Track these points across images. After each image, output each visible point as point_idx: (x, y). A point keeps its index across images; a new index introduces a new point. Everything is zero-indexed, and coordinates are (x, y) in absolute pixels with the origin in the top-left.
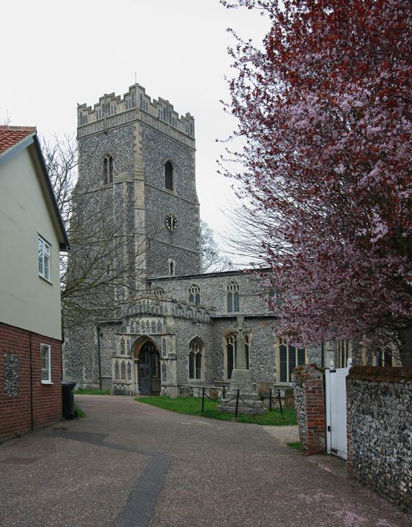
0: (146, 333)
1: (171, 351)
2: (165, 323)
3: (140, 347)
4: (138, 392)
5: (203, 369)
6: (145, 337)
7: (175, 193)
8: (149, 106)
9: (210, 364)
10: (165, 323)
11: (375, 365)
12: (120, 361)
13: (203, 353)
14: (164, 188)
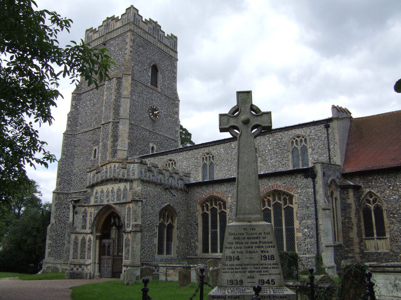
0: (111, 202)
1: (135, 221)
2: (131, 188)
4: (97, 274)
6: (108, 207)
7: (159, 90)
8: (141, 22)
9: (183, 236)
12: (80, 237)
13: (175, 225)
14: (149, 84)
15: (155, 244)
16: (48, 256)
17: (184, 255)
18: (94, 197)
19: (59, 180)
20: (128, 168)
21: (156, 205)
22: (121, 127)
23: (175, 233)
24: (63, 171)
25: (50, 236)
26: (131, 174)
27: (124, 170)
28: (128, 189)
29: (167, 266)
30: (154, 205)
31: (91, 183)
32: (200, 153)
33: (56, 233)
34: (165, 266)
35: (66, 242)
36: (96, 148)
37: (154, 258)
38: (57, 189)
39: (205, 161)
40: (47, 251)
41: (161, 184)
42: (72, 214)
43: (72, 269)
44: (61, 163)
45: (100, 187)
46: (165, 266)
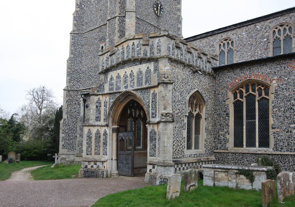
0: (130, 89)
2: (156, 69)
3: (120, 110)
5: (203, 135)
6: (127, 94)
10: (156, 69)
11: (48, 155)
12: (94, 130)
13: (203, 115)
15: (184, 138)
16: (62, 148)
17: (211, 149)
18: (108, 83)
19: (69, 78)
20: (151, 43)
21: (184, 90)
22: (127, 20)
23: (203, 124)
24: (72, 69)
25: (63, 130)
26: (155, 51)
27: (146, 47)
28: (152, 70)
29: (215, 168)
30: (182, 90)
31: (105, 68)
32: (216, 40)
33: (68, 127)
34: (213, 168)
35: (78, 136)
36: (103, 45)
37: (183, 154)
38: (67, 86)
39: (222, 48)
40: (61, 143)
41: (189, 66)
42: (83, 108)
43: (86, 167)
44: (70, 62)
45: (115, 71)
46: (213, 168)
